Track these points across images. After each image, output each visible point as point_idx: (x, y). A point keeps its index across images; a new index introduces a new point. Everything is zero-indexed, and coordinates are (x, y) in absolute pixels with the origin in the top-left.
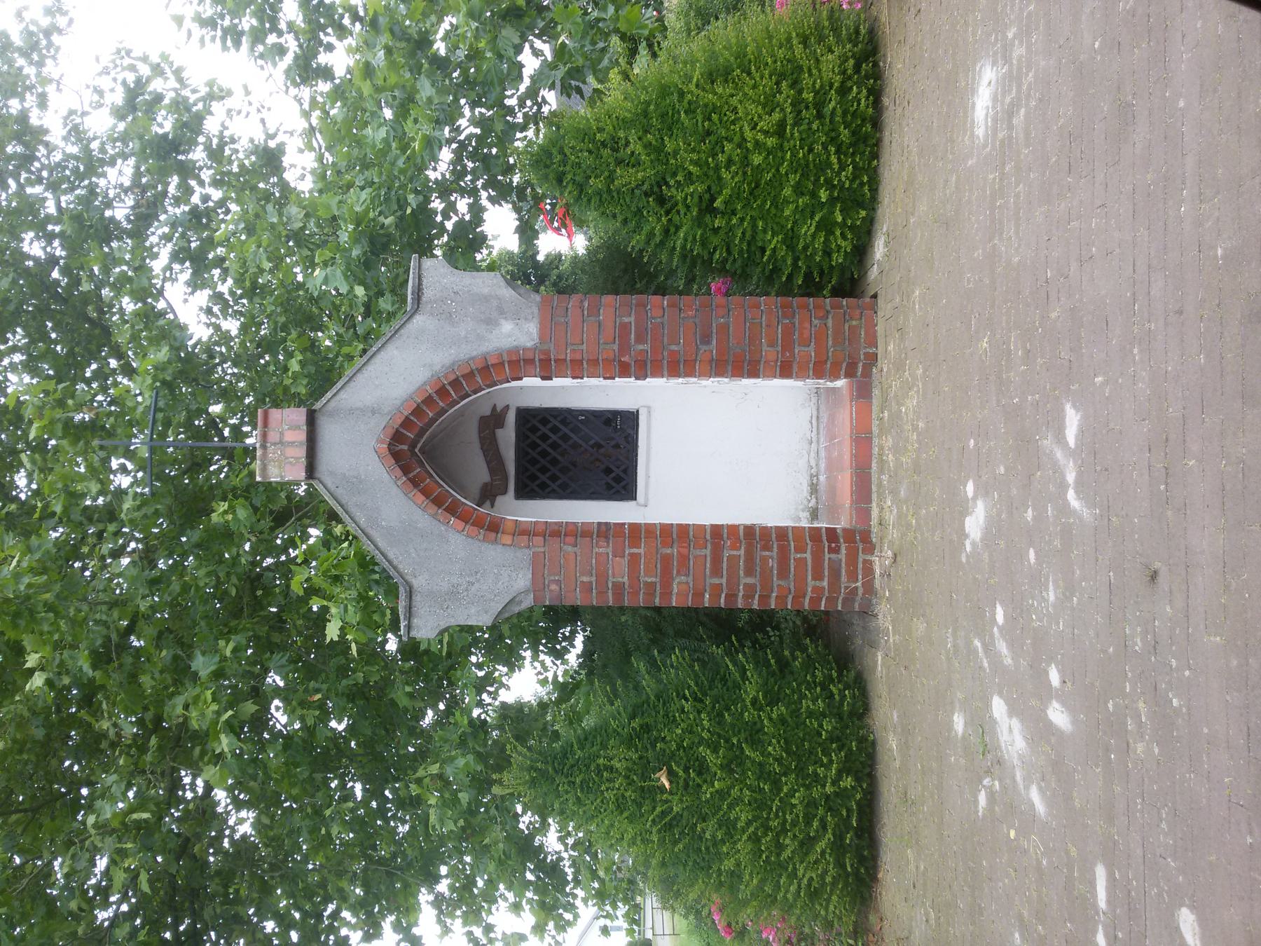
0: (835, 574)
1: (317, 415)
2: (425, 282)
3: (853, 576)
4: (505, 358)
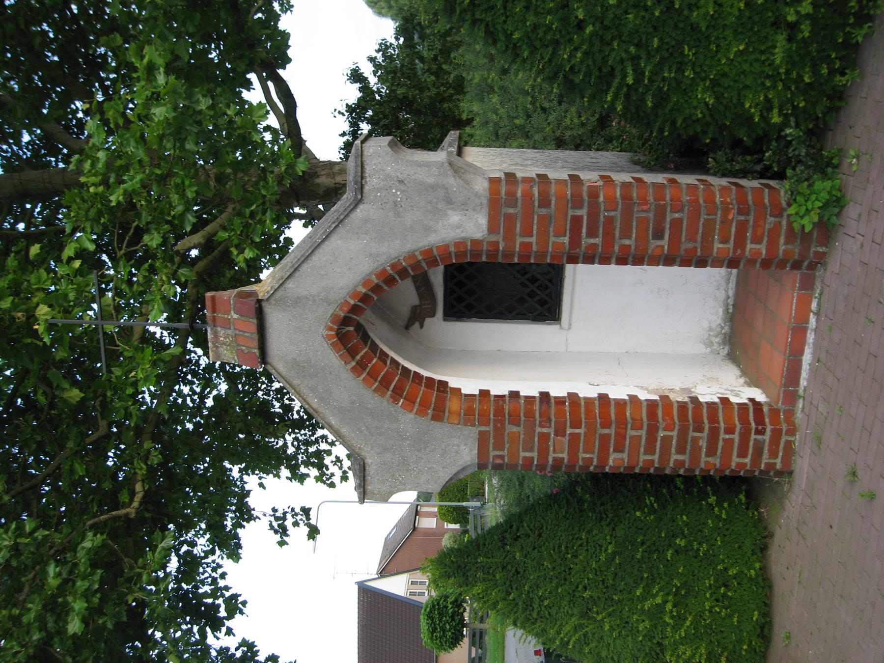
0: (758, 451)
1: (264, 304)
2: (368, 169)
3: (773, 454)
4: (452, 249)
